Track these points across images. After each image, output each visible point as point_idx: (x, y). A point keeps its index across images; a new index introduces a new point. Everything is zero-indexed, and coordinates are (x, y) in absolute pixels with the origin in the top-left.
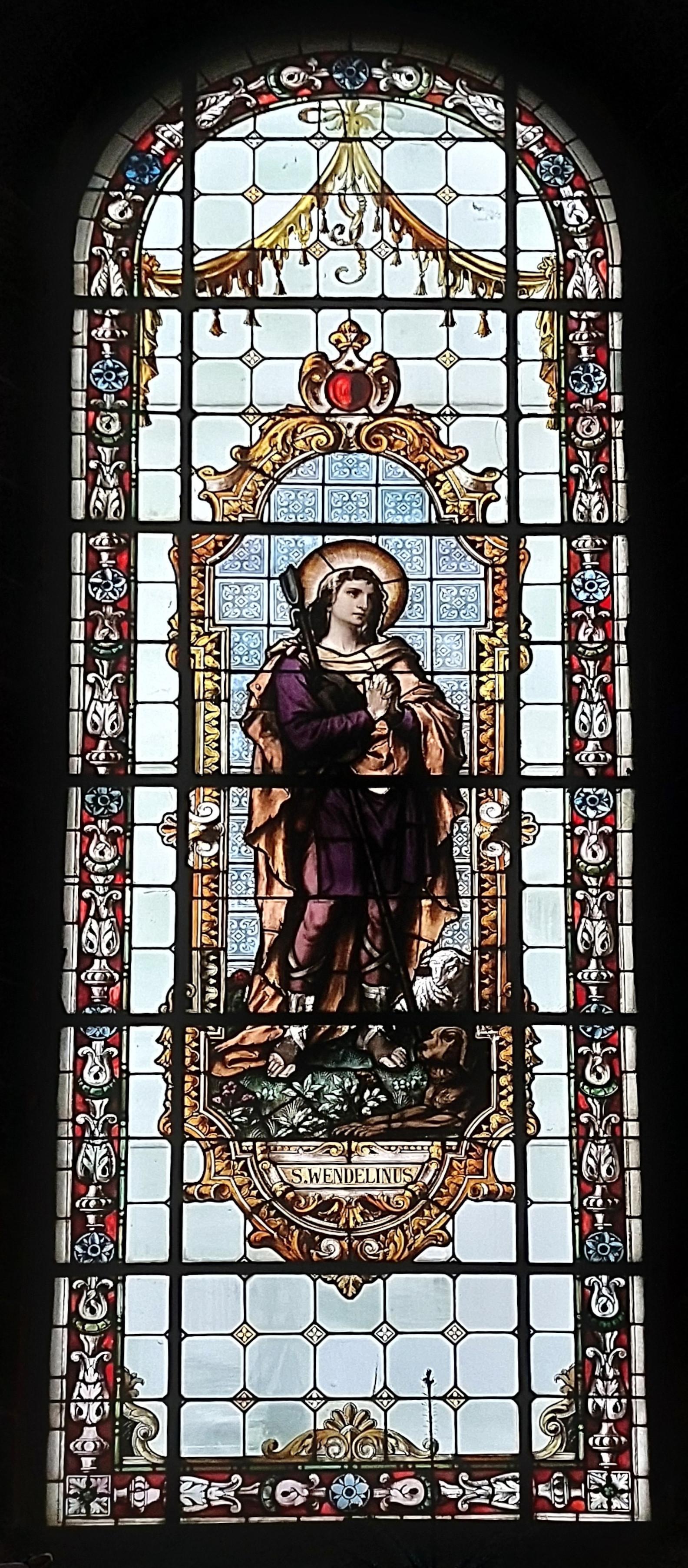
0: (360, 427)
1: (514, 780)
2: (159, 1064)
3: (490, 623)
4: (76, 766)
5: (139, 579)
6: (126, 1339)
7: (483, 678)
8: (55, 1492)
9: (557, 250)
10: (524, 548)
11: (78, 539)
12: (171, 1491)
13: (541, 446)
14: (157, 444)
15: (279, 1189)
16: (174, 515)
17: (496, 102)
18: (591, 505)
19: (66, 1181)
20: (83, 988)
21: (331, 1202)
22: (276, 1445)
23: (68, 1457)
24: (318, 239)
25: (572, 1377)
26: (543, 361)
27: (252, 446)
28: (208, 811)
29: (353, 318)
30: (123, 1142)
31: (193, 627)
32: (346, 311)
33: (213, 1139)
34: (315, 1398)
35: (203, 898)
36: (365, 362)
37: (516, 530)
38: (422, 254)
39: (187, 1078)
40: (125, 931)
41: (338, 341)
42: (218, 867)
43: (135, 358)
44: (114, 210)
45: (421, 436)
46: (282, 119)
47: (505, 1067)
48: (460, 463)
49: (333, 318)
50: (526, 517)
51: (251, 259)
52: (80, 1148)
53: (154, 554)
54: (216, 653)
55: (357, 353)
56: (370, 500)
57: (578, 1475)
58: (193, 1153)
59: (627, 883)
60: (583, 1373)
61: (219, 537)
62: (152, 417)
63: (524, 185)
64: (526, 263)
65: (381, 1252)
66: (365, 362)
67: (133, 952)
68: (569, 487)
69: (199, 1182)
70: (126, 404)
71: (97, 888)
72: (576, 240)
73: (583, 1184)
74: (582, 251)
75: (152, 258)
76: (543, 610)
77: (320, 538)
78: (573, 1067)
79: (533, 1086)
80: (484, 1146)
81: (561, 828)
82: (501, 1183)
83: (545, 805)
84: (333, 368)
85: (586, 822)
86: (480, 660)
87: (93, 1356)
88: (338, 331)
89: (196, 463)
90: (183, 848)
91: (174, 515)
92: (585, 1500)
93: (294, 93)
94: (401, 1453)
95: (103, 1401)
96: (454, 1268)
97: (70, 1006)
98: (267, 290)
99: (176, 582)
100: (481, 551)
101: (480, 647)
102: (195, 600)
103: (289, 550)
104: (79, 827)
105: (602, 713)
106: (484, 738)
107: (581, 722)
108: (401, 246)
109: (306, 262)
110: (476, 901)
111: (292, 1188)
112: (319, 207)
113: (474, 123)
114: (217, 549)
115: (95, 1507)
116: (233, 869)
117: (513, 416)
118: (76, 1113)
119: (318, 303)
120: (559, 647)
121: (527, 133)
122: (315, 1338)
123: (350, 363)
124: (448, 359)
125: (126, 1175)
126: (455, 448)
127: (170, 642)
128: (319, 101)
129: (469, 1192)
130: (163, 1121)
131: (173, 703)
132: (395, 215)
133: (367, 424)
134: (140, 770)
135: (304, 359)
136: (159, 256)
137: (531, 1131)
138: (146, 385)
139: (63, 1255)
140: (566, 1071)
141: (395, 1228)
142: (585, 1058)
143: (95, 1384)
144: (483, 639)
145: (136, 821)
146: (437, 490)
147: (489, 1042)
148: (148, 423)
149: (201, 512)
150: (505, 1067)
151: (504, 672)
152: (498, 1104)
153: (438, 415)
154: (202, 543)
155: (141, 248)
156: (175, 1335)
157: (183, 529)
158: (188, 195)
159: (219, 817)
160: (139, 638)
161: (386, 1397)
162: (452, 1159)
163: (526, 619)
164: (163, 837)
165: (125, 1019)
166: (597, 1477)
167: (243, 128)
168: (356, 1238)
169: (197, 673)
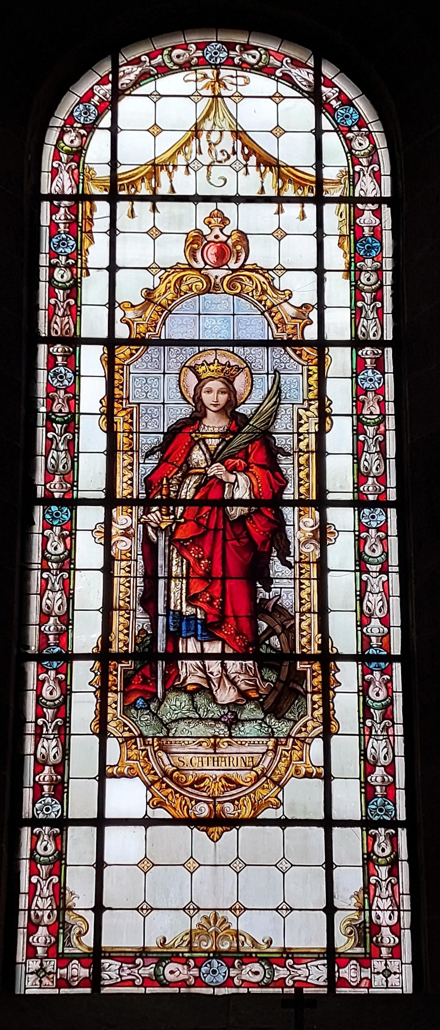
0: (224, 277)
1: (322, 502)
3: (306, 403)
4: (40, 492)
5: (82, 374)
6: (68, 868)
7: (302, 437)
10: (327, 354)
11: (42, 349)
12: (97, 970)
13: (338, 290)
14: (94, 289)
15: (170, 769)
17: (308, 73)
19: (30, 763)
20: (43, 636)
21: (203, 779)
22: (165, 940)
23: (31, 945)
24: (196, 159)
26: (340, 236)
28: (125, 521)
29: (219, 208)
31: (116, 405)
34: (191, 909)
36: (226, 236)
37: (322, 344)
38: (263, 168)
41: (210, 223)
42: (131, 557)
43: (79, 232)
47: (316, 689)
48: (286, 301)
49: (206, 208)
51: (155, 168)
53: (91, 359)
54: (130, 421)
55: (221, 230)
57: (366, 962)
58: (112, 745)
59: (397, 569)
60: (369, 894)
63: (326, 124)
64: (329, 174)
66: (226, 236)
68: (357, 314)
69: (117, 765)
72: (360, 160)
73: (368, 766)
74: (364, 166)
76: (340, 393)
77: (197, 348)
79: (335, 700)
80: (303, 742)
81: (351, 456)
82: (315, 766)
83: (342, 519)
85: (367, 530)
86: (300, 425)
88: (210, 217)
89: (119, 298)
90: (108, 546)
91: (104, 334)
94: (247, 947)
96: (283, 823)
97: (34, 647)
98: (163, 190)
99: (105, 376)
100: (300, 356)
101: (300, 417)
102: (118, 387)
104: (41, 532)
105: (377, 459)
106: (302, 475)
107: (367, 606)
108: (249, 163)
110: (297, 581)
111: (178, 770)
113: (294, 86)
114: (132, 355)
115: (45, 981)
116: (143, 467)
118: (37, 718)
119: (196, 199)
123: (217, 237)
124: (280, 234)
125: (69, 760)
126: (284, 291)
127: (102, 414)
130: (93, 724)
134: (81, 495)
135: (187, 234)
137: (334, 730)
138: (87, 250)
141: (245, 796)
144: (301, 412)
146: (272, 317)
147: (305, 672)
148: (88, 274)
149: (122, 332)
150: (316, 689)
151: (316, 433)
153: (272, 270)
154: (122, 352)
155: (84, 162)
156: (100, 865)
157: (110, 343)
158: (114, 130)
160: (81, 411)
163: (329, 400)
165: (69, 657)
166: (378, 965)
167: (147, 88)
168: (219, 802)
169: (119, 434)
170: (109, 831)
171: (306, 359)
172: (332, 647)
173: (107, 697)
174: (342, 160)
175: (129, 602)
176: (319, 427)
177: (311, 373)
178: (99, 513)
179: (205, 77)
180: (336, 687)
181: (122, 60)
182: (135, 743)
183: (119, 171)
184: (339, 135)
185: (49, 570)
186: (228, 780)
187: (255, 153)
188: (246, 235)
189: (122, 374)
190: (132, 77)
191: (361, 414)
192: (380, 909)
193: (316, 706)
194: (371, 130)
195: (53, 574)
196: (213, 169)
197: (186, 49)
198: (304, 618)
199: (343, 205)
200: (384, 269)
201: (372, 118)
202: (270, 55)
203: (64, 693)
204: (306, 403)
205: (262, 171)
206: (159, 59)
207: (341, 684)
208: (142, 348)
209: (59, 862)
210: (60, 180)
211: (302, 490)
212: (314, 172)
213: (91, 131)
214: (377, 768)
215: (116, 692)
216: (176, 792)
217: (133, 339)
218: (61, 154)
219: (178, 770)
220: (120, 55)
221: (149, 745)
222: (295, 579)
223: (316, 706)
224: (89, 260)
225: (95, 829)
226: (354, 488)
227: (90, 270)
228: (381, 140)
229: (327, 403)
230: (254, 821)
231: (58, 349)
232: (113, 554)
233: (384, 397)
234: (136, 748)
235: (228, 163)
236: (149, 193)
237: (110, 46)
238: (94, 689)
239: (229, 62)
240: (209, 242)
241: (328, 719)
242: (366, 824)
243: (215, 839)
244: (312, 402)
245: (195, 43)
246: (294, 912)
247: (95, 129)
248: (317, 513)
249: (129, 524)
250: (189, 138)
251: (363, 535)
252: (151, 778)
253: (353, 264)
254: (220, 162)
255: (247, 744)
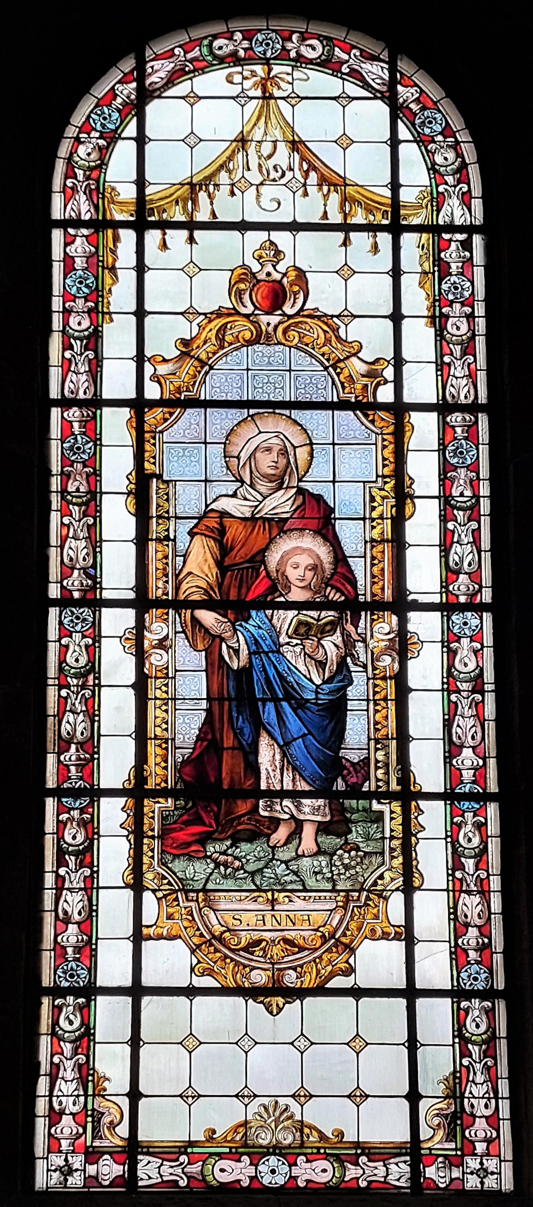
1: (401, 604)
2: (124, 828)
4: (54, 591)
6: (97, 1045)
7: (374, 524)
8: (41, 1166)
9: (431, 186)
10: (408, 422)
13: (419, 339)
14: (118, 338)
15: (218, 929)
16: (132, 395)
18: (461, 390)
20: (63, 768)
22: (214, 1132)
25: (451, 1082)
27: (192, 339)
29: (271, 238)
30: (95, 891)
32: (267, 233)
33: (166, 890)
35: (156, 698)
37: (400, 410)
39: (146, 841)
40: (95, 721)
41: (261, 257)
42: (167, 674)
43: (100, 269)
44: (82, 150)
45: (325, 332)
46: (213, 81)
48: (355, 355)
50: (408, 398)
51: (193, 188)
52: (61, 894)
53: (115, 424)
55: (274, 267)
56: (285, 382)
58: (148, 898)
61: (166, 410)
62: (113, 316)
63: (404, 133)
64: (407, 196)
65: (299, 980)
67: (102, 738)
69: (155, 924)
70: (93, 305)
71: (72, 688)
72: (446, 177)
73: (459, 926)
75: (113, 189)
76: (423, 470)
78: (449, 834)
79: (417, 848)
80: (380, 896)
84: (255, 278)
86: (373, 509)
87: (71, 1059)
89: (148, 353)
90: (141, 656)
92: (463, 1180)
93: (222, 60)
95: (78, 1096)
96: (357, 993)
98: (202, 216)
100: (373, 422)
101: (373, 499)
103: (221, 420)
107: (457, 733)
109: (233, 194)
111: (229, 930)
112: (243, 149)
113: (366, 86)
114: (166, 420)
117: (397, 317)
119: (243, 226)
120: (437, 500)
121: (405, 93)
122: (246, 1046)
123: (269, 274)
124: (346, 272)
126: (351, 343)
128: (242, 66)
129: (367, 932)
131: (132, 541)
132: (303, 159)
133: (283, 323)
134: (107, 595)
135: (232, 271)
136: (119, 187)
137: (417, 883)
138: (110, 290)
139: (46, 981)
140: (444, 836)
142: (459, 826)
143: (72, 1081)
145: (103, 634)
146: (338, 374)
148: (112, 320)
149: (152, 392)
152: (390, 864)
157: (139, 405)
158: (141, 140)
159: (168, 634)
161: (303, 1096)
162: (354, 907)
163: (410, 478)
164: (124, 647)
165: (95, 794)
167: (182, 88)
170: (147, 980)
171: (381, 426)
172: (415, 782)
173: (142, 844)
174: (424, 178)
175: (166, 730)
176: (397, 512)
177: (385, 443)
178: (128, 617)
179: (254, 74)
180: (419, 832)
181: (149, 53)
182: (176, 899)
183: (149, 191)
184: (420, 147)
185: (68, 686)
186: (286, 941)
187: (315, 169)
188: (305, 272)
189: (154, 445)
190: (162, 74)
191: (450, 495)
192: (474, 1097)
193: (395, 854)
194: (460, 140)
195: (73, 692)
196: (263, 189)
197: (231, 39)
198: (374, 524)
199: (425, 236)
200: (476, 314)
201: (460, 126)
202: (335, 46)
203: (90, 837)
204: (380, 479)
205: (325, 192)
206: (195, 53)
207: (424, 829)
208: (179, 410)
209: (86, 1037)
210: (75, 203)
211: (377, 589)
212: (390, 192)
213: (112, 141)
214: (470, 928)
215: (153, 837)
216: (226, 957)
217: (166, 400)
218: (76, 170)
219: (229, 930)
220: (147, 47)
221: (192, 900)
222: (368, 700)
223: (395, 854)
224: (111, 302)
225: (130, 999)
226: (442, 587)
227: (113, 316)
228: (469, 152)
229: (408, 482)
230: (321, 991)
231: (74, 413)
232: (146, 671)
233: (478, 474)
234: (178, 905)
235: (284, 181)
236: (183, 218)
237: (134, 42)
238: (126, 833)
239: (283, 56)
240: (259, 281)
241: (409, 869)
242: (457, 994)
243: (275, 1013)
244: (388, 480)
245: (240, 31)
246: (370, 1098)
247: (117, 139)
248: (395, 618)
249: (164, 633)
250: (234, 151)
251: (454, 645)
252: (196, 940)
253: (437, 309)
254: (274, 180)
255: (312, 900)
